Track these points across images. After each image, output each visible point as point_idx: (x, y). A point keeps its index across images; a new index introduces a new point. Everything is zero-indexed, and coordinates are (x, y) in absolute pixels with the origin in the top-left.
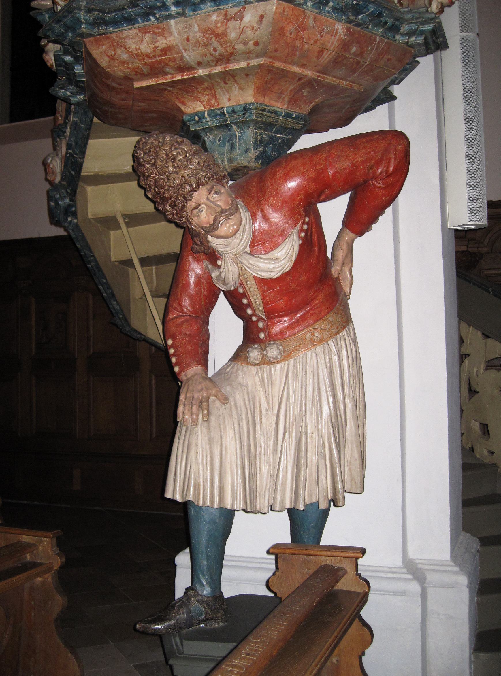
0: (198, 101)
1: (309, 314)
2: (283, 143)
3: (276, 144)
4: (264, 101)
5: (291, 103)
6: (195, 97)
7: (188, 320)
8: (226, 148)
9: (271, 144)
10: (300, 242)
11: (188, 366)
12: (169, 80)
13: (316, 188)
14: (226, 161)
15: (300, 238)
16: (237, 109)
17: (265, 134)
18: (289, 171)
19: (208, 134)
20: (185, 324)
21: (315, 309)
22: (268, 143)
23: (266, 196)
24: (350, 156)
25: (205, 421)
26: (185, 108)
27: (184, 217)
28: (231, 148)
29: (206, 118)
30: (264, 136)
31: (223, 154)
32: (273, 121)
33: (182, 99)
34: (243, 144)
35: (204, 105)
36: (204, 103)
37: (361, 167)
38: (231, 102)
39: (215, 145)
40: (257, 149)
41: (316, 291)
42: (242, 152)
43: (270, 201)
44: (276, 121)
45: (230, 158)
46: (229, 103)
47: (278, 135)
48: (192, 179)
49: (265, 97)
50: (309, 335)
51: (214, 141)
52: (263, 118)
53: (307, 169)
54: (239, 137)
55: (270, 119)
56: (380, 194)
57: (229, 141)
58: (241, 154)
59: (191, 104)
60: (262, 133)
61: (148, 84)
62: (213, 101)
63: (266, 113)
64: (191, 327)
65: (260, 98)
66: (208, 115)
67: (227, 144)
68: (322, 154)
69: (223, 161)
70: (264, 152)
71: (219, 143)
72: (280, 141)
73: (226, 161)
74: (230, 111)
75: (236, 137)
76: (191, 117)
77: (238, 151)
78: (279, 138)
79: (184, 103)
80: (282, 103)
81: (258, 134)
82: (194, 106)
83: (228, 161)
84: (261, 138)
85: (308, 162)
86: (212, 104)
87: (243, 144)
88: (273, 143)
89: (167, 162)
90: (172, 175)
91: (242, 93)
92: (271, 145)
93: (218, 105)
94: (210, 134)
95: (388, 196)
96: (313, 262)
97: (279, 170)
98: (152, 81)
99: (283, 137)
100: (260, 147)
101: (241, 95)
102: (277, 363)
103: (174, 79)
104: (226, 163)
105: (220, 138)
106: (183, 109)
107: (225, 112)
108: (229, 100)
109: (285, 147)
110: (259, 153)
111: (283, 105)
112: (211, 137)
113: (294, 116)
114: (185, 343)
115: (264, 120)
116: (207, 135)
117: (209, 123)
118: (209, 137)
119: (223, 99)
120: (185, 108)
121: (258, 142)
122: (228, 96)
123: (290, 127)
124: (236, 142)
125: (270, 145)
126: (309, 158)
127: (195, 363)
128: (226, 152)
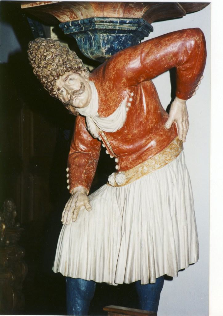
0: (65, 15)
1: (143, 155)
2: (127, 39)
3: (121, 41)
4: (103, 15)
5: (126, 12)
6: (62, 13)
7: (79, 156)
8: (88, 46)
9: (116, 41)
10: (127, 109)
11: (74, 186)
12: (38, 5)
13: (133, 75)
14: (89, 53)
15: (127, 106)
16: (86, 21)
17: (110, 35)
18: (116, 64)
19: (77, 36)
20: (77, 158)
21: (147, 151)
22: (114, 41)
23: (105, 80)
24: (155, 52)
25: (74, 222)
26: (60, 19)
27: (55, 94)
28: (90, 45)
29: (71, 27)
30: (110, 37)
31: (86, 49)
32: (112, 28)
33: (56, 14)
34: (96, 43)
35: (69, 18)
36: (69, 16)
37: (164, 59)
38: (83, 16)
39: (81, 43)
40: (105, 46)
41: (148, 139)
42: (96, 48)
43: (107, 83)
44: (115, 27)
45: (91, 52)
46: (83, 17)
47: (121, 35)
48: (54, 72)
49: (103, 12)
50: (140, 169)
51: (80, 41)
52: (103, 27)
53: (126, 62)
54: (94, 39)
55: (109, 26)
56: (184, 74)
57: (88, 42)
58: (96, 50)
59: (62, 16)
60: (108, 35)
61: (28, 7)
62: (74, 15)
63: (105, 24)
64: (80, 160)
65: (100, 13)
66: (71, 25)
67: (88, 43)
68: (137, 52)
69: (88, 54)
70: (111, 47)
71: (83, 42)
72: (123, 38)
73: (89, 53)
74: (82, 23)
75: (92, 38)
76: (63, 26)
77: (94, 48)
78: (123, 36)
79: (58, 16)
80: (118, 14)
81: (105, 36)
82: (64, 18)
83: (90, 54)
84: (108, 39)
85: (128, 57)
86: (74, 17)
87: (96, 43)
88: (118, 41)
89: (41, 61)
90: (44, 69)
91: (87, 10)
92: (116, 42)
93: (77, 18)
94: (78, 36)
95: (190, 75)
96: (142, 121)
97: (111, 63)
98: (30, 5)
99: (126, 36)
100: (107, 45)
101: (87, 12)
102: (122, 186)
103: (41, 5)
104: (90, 55)
105: (83, 39)
106: (59, 19)
107: (80, 23)
108: (82, 15)
109: (128, 42)
110: (108, 49)
111: (120, 15)
112: (79, 38)
113: (128, 22)
114: (75, 171)
115: (104, 28)
116: (76, 37)
117: (74, 30)
118: (78, 38)
119: (78, 14)
120: (60, 19)
121: (106, 42)
122: (80, 13)
123: (126, 29)
124: (92, 42)
125: (115, 42)
126: (129, 55)
127: (78, 184)
128: (88, 48)
